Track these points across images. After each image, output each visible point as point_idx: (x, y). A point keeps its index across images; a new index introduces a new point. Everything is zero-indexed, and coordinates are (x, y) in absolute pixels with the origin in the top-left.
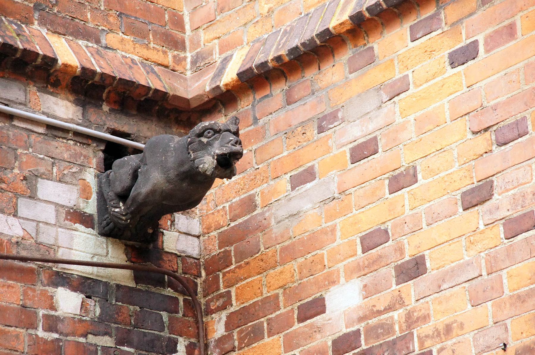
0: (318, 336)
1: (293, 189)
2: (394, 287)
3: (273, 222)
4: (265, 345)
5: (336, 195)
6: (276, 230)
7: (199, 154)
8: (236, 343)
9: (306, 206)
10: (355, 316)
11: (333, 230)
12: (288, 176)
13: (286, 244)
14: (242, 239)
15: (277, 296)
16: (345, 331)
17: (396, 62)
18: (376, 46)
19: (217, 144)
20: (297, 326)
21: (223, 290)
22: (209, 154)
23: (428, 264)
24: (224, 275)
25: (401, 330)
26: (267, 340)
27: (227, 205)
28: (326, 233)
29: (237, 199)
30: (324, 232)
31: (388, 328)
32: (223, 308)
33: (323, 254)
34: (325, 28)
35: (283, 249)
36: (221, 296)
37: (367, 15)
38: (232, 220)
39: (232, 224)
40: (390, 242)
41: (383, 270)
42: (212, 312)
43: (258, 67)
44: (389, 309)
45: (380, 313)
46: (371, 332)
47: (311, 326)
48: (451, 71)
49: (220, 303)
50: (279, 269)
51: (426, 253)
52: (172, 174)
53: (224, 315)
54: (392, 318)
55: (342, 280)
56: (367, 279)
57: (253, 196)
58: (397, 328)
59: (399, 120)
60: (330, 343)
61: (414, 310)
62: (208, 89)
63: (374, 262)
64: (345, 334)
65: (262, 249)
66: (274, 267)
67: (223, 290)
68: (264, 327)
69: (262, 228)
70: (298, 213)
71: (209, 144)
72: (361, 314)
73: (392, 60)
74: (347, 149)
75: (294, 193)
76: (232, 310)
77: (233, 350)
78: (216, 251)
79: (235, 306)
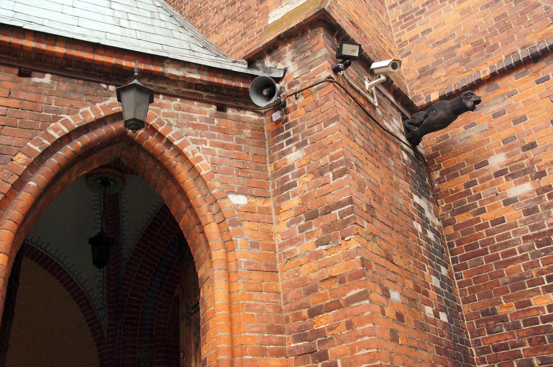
0: (486, 172)
2: (522, 153)
4: (460, 178)
7: (466, 101)
8: (446, 179)
9: (473, 134)
10: (504, 164)
12: (463, 126)
13: (466, 146)
14: (444, 147)
17: (509, 86)
19: (473, 97)
20: (475, 171)
21: (436, 164)
22: (470, 101)
23: (538, 144)
26: (460, 176)
27: (435, 138)
30: (484, 140)
31: (523, 166)
32: (438, 169)
33: (484, 148)
36: (437, 166)
38: (437, 143)
39: (438, 144)
42: (433, 171)
43: (448, 94)
45: (516, 162)
46: (511, 169)
47: (482, 170)
48: (537, 85)
50: (463, 154)
51: (537, 141)
52: (449, 111)
53: (438, 172)
54: (523, 162)
55: (495, 154)
58: (526, 165)
61: (534, 159)
64: (500, 170)
65: (454, 149)
66: (460, 154)
67: (436, 164)
68: (218, 142)
69: (453, 143)
70: (470, 136)
71: (470, 98)
72: (507, 163)
73: (507, 86)
74: (490, 114)
75: (467, 131)
76: (442, 169)
77: (445, 181)
79: (443, 168)
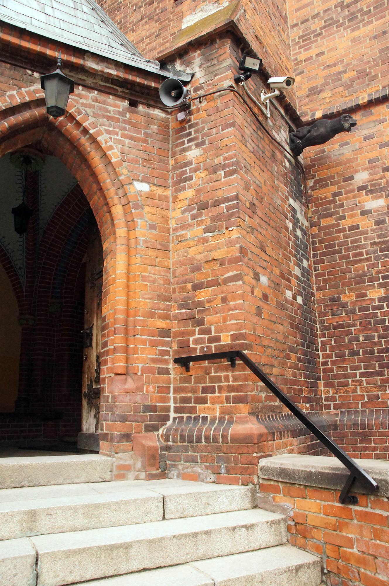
0: (351, 186)
1: (340, 147)
3: (332, 156)
5: (358, 149)
6: (333, 158)
9: (346, 152)
11: (357, 158)
12: (338, 144)
14: (320, 160)
15: (334, 176)
16: (362, 185)
18: (373, 111)
20: (342, 183)
21: (312, 174)
24: (313, 170)
25: (384, 185)
26: (330, 187)
28: (354, 159)
29: (318, 150)
32: (313, 178)
34: (11, 210)
35: (336, 163)
36: (312, 175)
37: (374, 101)
40: (380, 161)
41: (377, 169)
44: (380, 179)
45: (376, 180)
49: (312, 177)
52: (329, 129)
53: (313, 180)
55: (361, 171)
56: (370, 171)
57: (324, 149)
58: (383, 184)
59: (382, 129)
60: (356, 188)
62: (335, 111)
63: (373, 167)
65: (328, 163)
71: (348, 120)
72: (369, 180)
76: (316, 179)
77: (317, 189)
78: (309, 163)
79: (317, 178)
